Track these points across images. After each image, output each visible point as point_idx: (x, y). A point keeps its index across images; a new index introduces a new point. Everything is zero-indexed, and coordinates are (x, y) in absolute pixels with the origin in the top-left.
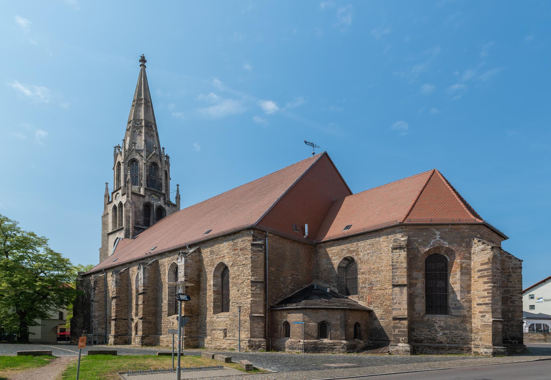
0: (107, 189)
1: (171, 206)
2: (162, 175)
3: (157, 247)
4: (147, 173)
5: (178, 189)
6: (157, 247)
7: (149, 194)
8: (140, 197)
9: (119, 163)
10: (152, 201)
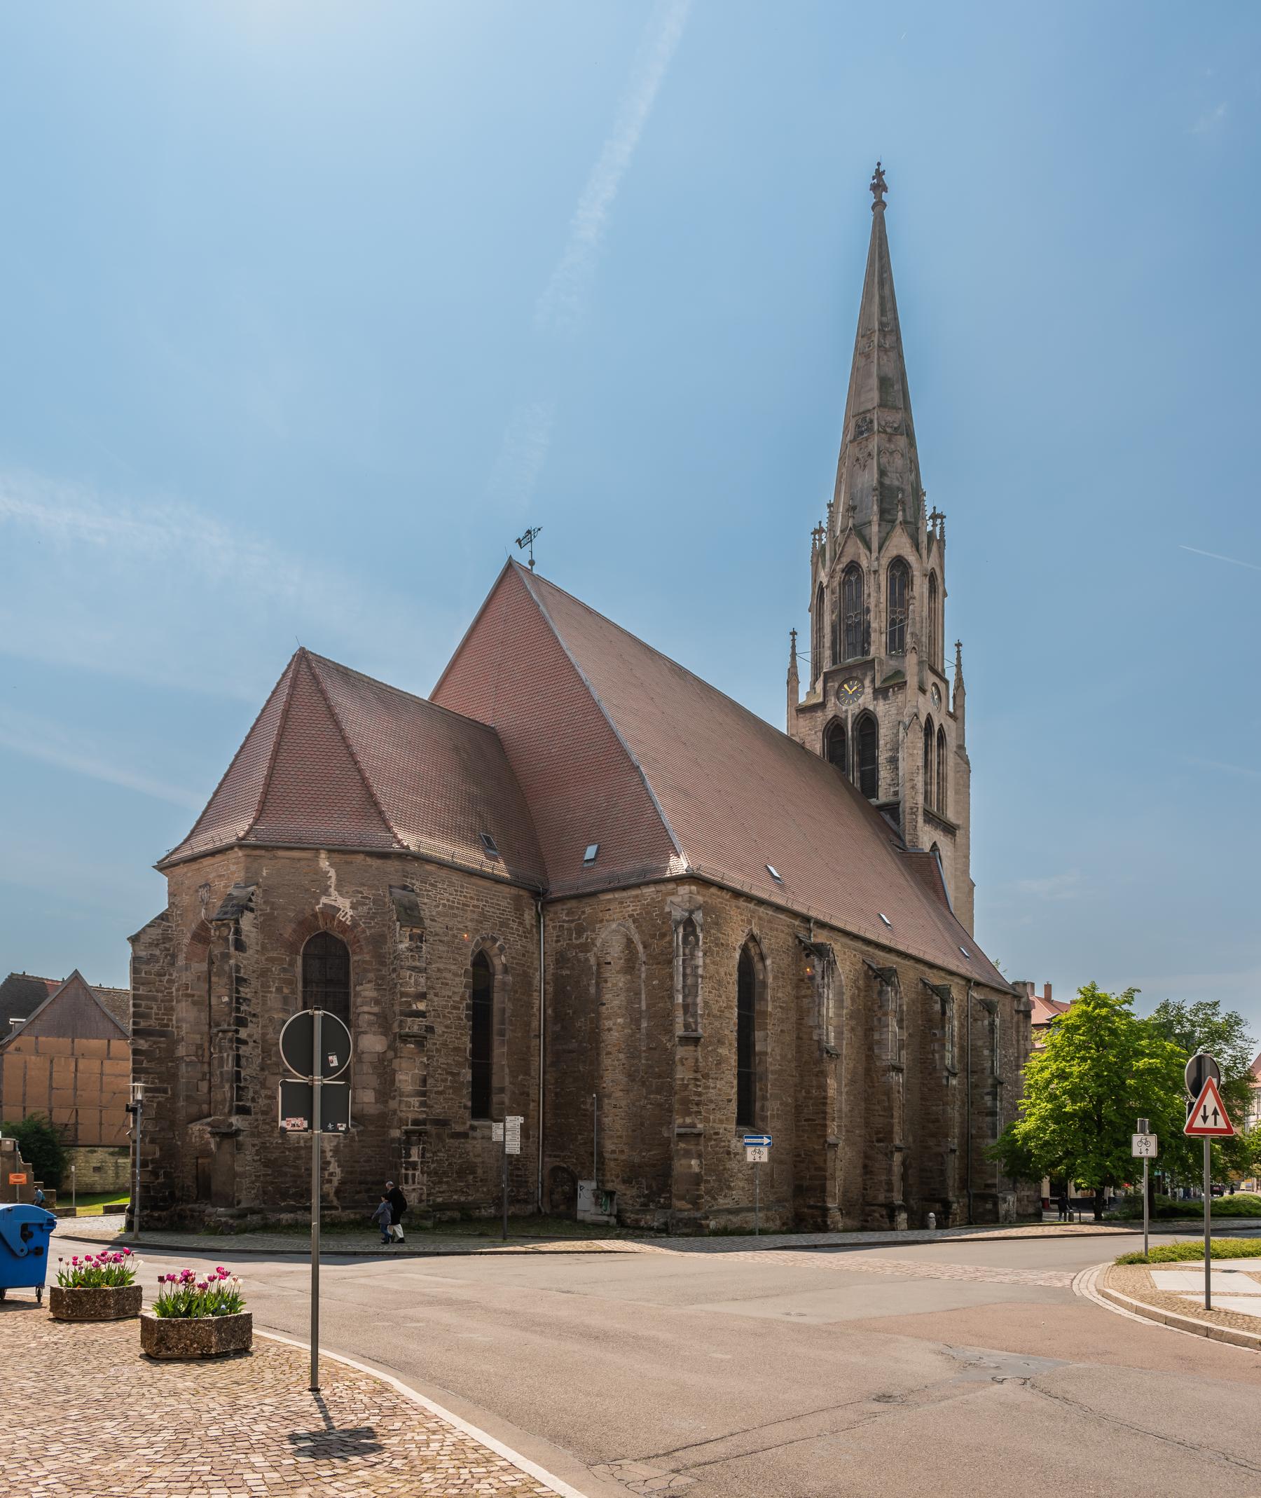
0: (794, 655)
1: (893, 691)
2: (869, 595)
3: (879, 186)
4: (834, 616)
5: (959, 658)
6: (879, 186)
7: (836, 685)
8: (816, 712)
9: (821, 590)
10: (844, 708)
